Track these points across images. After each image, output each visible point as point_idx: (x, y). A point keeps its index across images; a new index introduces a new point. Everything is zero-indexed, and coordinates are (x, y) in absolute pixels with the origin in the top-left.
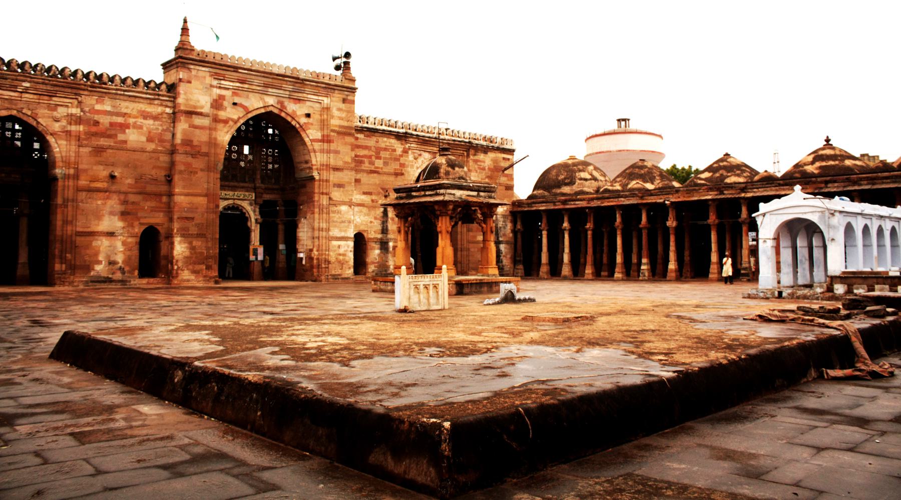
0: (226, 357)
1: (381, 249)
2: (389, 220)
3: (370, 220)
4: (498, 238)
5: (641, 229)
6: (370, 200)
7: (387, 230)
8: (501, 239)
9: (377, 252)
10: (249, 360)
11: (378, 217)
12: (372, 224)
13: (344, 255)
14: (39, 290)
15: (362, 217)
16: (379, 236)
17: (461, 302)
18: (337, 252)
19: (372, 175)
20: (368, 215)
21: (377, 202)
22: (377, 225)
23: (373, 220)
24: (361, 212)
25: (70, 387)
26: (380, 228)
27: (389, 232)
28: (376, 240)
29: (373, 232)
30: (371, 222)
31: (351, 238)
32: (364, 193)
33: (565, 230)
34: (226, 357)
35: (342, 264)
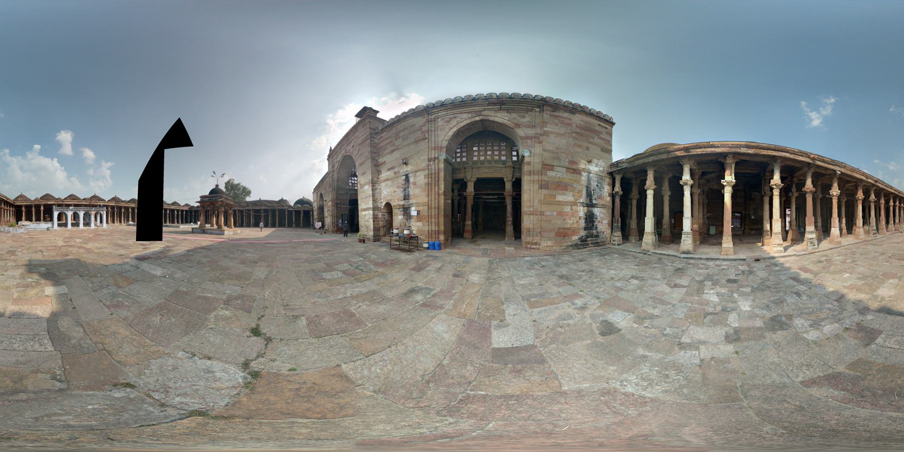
0: (109, 218)
1: (404, 215)
2: (411, 185)
3: (393, 190)
4: (591, 200)
5: (806, 193)
6: (393, 173)
7: (408, 195)
8: (594, 202)
9: (401, 217)
10: (615, 368)
11: (400, 185)
12: (396, 193)
13: (368, 221)
14: (861, 211)
15: (388, 190)
16: (402, 203)
17: (187, 238)
18: (364, 219)
19: (394, 153)
20: (391, 186)
21: (399, 172)
22: (400, 194)
23: (396, 189)
24: (387, 185)
25: (656, 356)
26: (402, 195)
27: (411, 197)
28: (399, 207)
29: (396, 200)
30: (395, 191)
31: (164, 232)
32: (388, 170)
33: (686, 184)
34: (109, 218)
35: (367, 227)
